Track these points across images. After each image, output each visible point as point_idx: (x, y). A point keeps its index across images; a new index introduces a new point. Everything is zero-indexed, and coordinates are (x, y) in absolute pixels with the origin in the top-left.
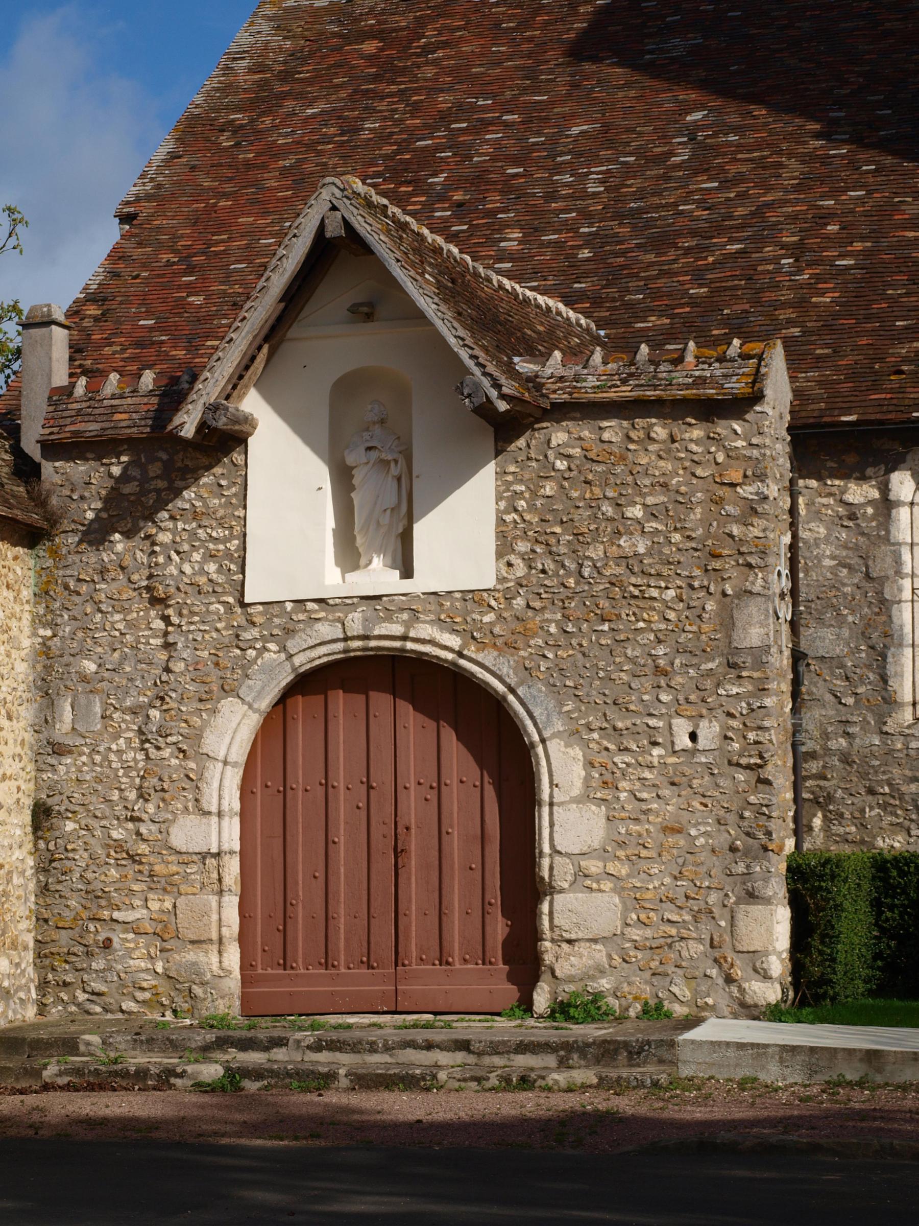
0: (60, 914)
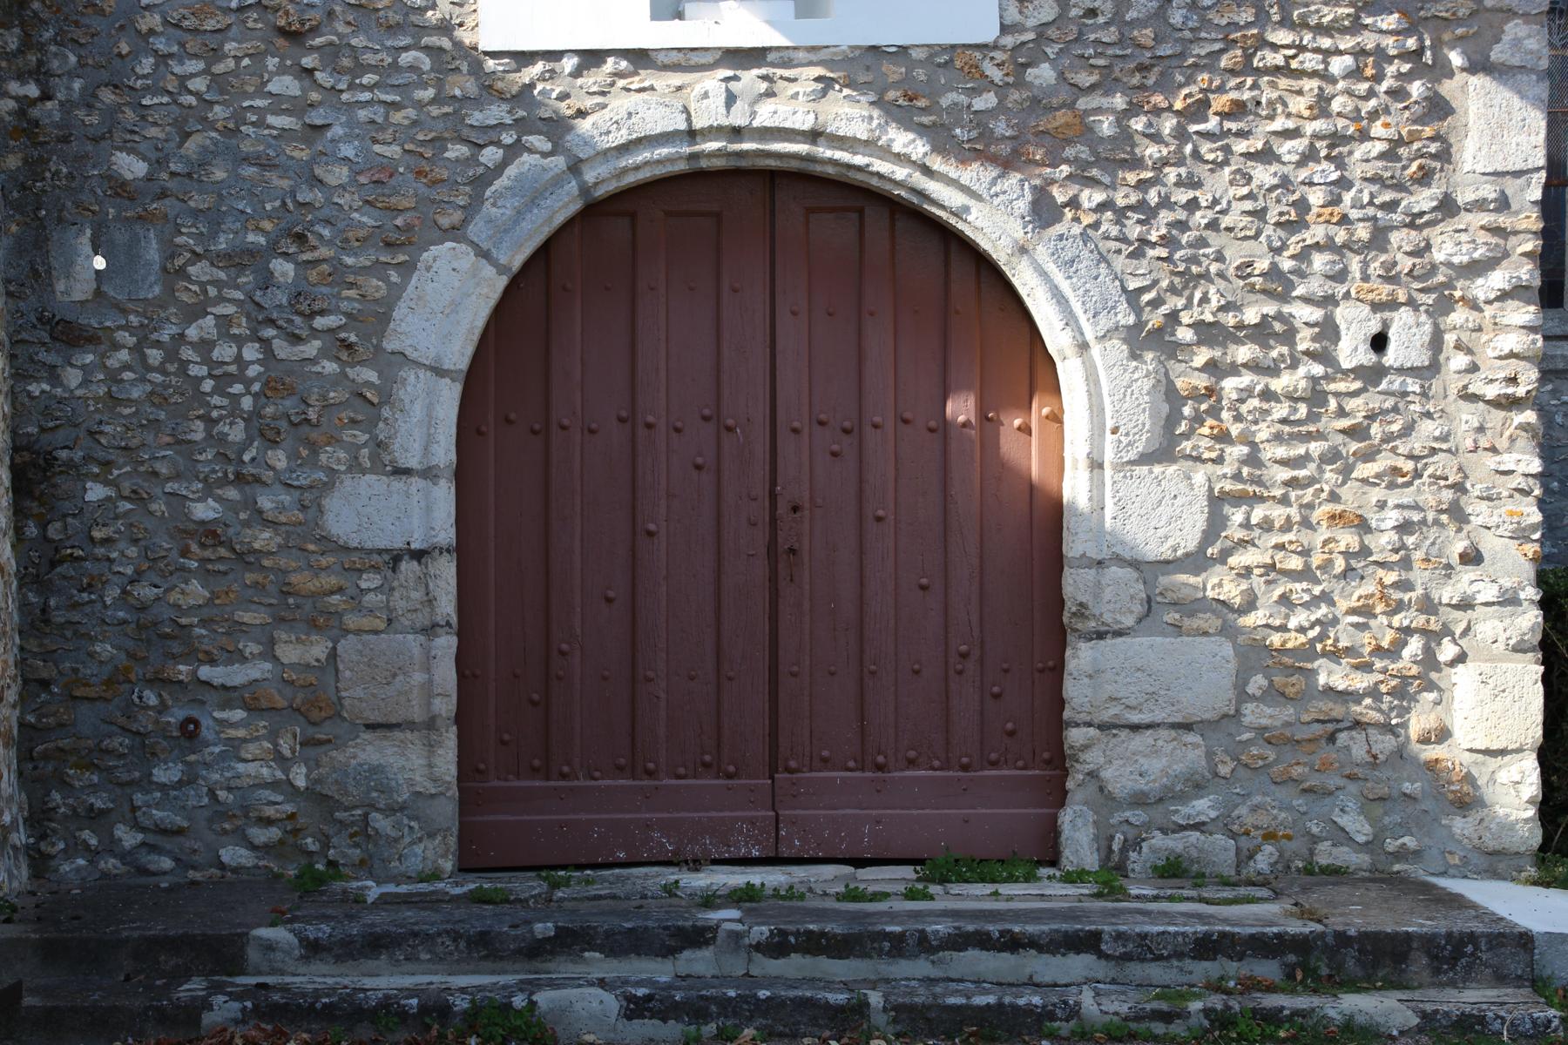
0: (76, 671)
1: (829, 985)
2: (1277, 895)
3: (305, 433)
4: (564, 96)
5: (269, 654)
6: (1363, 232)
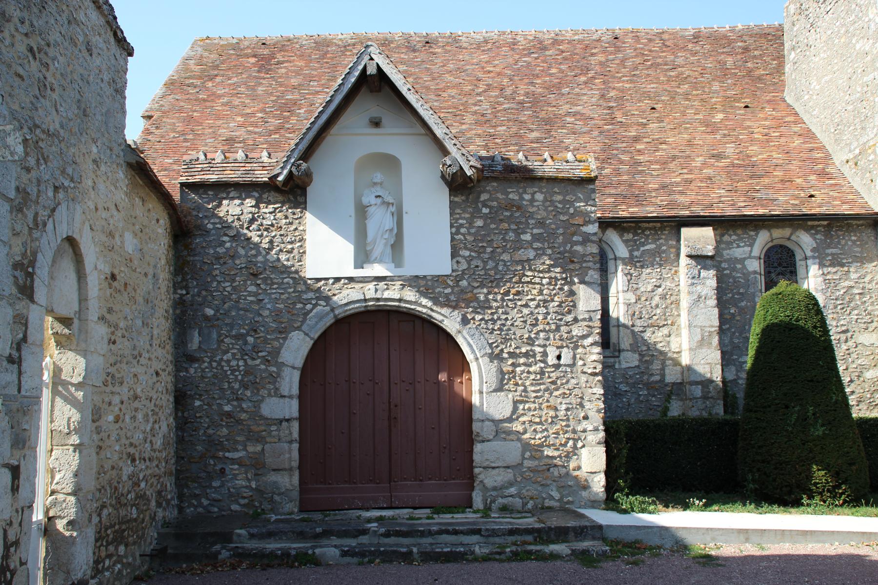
1: (402, 546)
2: (533, 515)
3: (256, 386)
4: (329, 290)
5: (245, 449)
6: (553, 327)
